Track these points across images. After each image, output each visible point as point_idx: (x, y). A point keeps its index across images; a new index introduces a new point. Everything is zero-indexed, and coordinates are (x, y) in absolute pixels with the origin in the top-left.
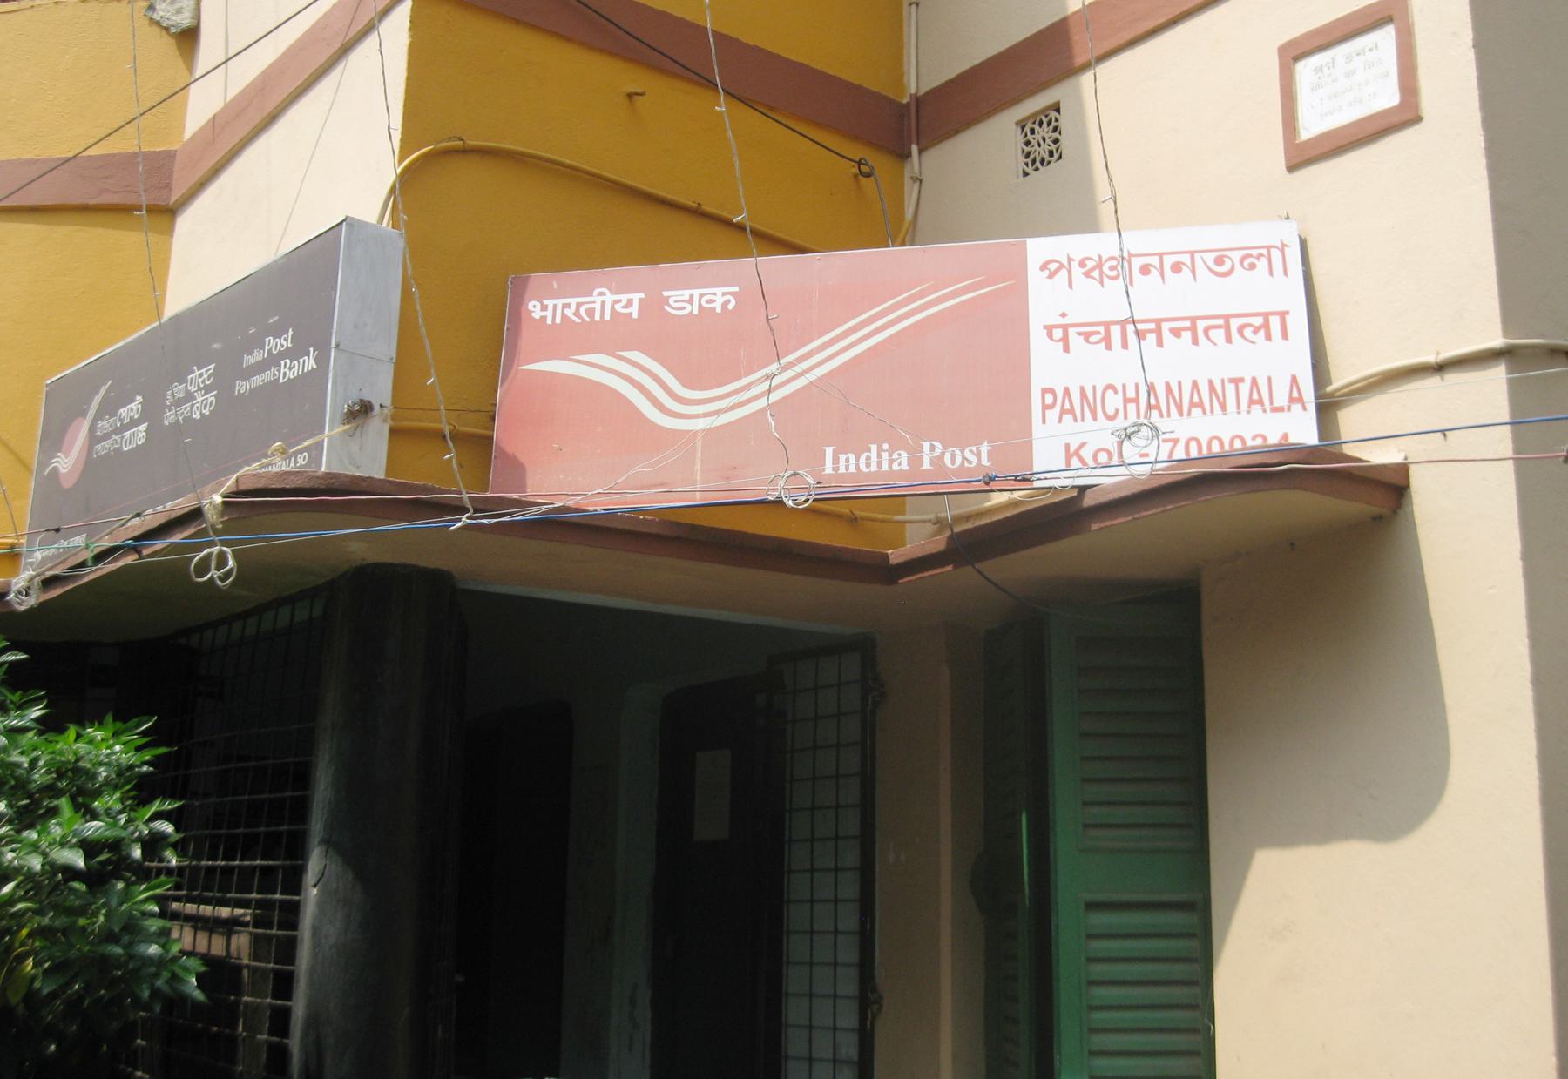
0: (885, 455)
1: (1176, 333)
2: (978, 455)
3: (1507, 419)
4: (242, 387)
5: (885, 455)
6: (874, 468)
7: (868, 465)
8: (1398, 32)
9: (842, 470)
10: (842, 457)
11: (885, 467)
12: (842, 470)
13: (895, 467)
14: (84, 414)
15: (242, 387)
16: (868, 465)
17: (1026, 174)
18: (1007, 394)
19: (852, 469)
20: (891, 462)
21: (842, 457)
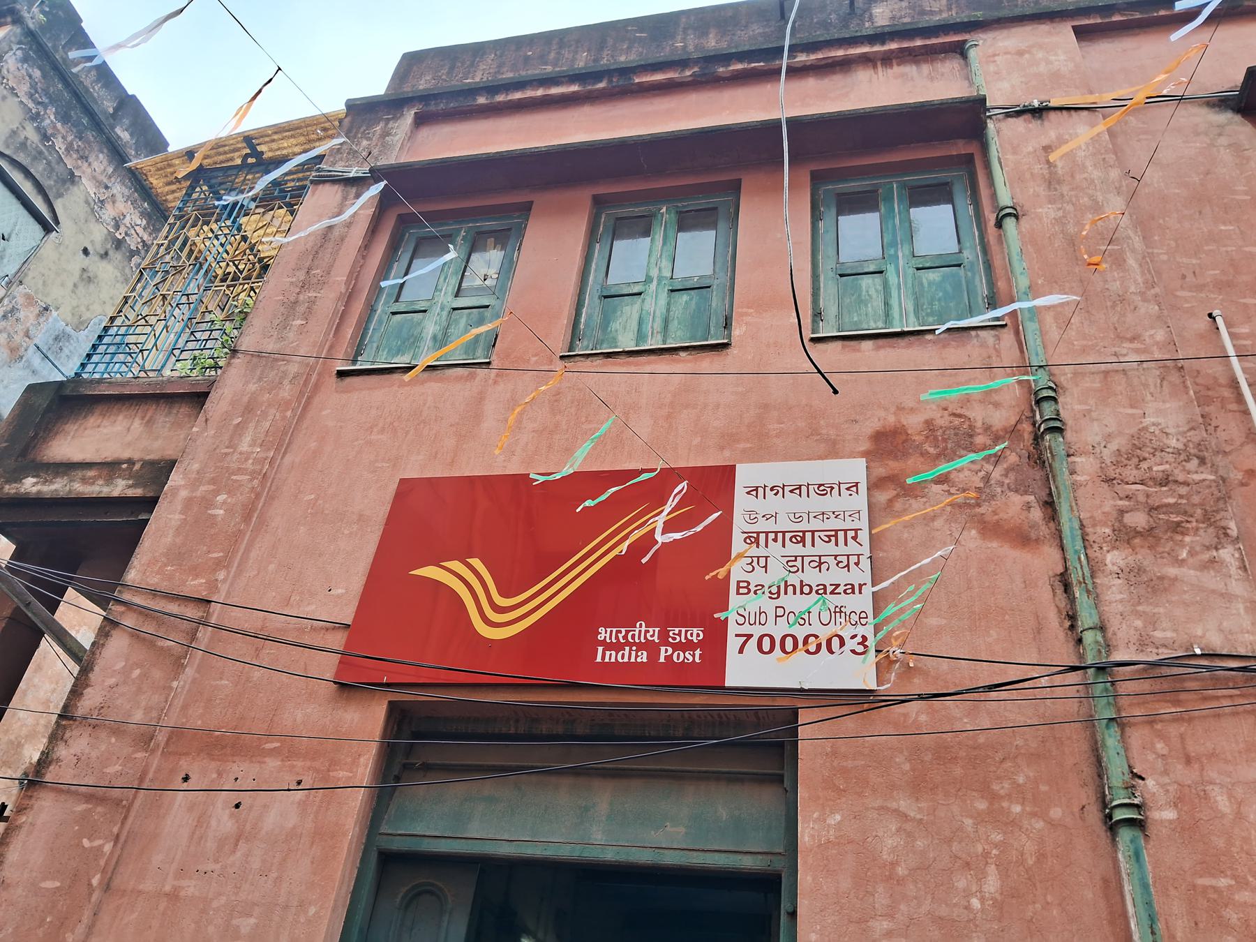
0: (633, 653)
1: (791, 491)
2: (694, 656)
3: (329, 675)
4: (600, 649)
5: (633, 653)
6: (626, 660)
7: (623, 657)
8: (7, 829)
9: (607, 660)
10: (608, 653)
11: (633, 660)
12: (607, 660)
13: (639, 660)
14: (1174, 706)
15: (600, 649)
16: (623, 657)
17: (748, 493)
18: (705, 608)
19: (613, 660)
20: (637, 656)
21: (608, 653)
